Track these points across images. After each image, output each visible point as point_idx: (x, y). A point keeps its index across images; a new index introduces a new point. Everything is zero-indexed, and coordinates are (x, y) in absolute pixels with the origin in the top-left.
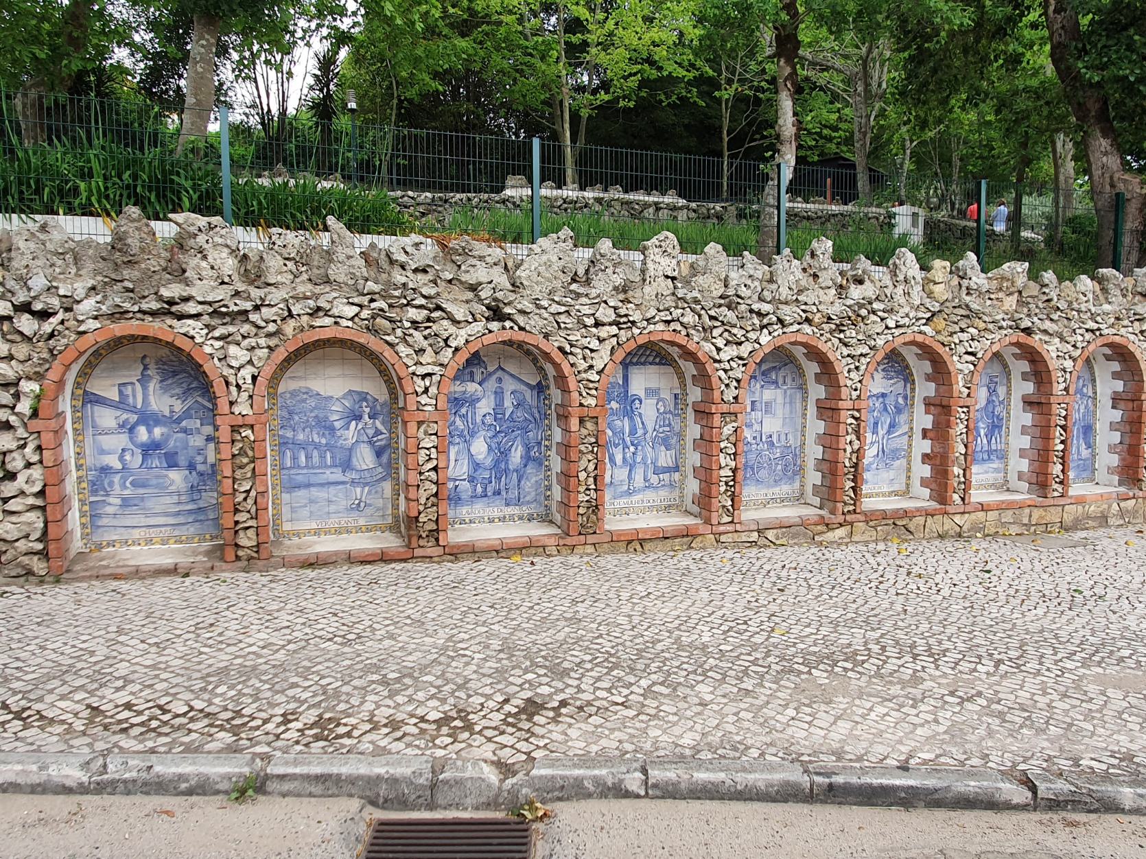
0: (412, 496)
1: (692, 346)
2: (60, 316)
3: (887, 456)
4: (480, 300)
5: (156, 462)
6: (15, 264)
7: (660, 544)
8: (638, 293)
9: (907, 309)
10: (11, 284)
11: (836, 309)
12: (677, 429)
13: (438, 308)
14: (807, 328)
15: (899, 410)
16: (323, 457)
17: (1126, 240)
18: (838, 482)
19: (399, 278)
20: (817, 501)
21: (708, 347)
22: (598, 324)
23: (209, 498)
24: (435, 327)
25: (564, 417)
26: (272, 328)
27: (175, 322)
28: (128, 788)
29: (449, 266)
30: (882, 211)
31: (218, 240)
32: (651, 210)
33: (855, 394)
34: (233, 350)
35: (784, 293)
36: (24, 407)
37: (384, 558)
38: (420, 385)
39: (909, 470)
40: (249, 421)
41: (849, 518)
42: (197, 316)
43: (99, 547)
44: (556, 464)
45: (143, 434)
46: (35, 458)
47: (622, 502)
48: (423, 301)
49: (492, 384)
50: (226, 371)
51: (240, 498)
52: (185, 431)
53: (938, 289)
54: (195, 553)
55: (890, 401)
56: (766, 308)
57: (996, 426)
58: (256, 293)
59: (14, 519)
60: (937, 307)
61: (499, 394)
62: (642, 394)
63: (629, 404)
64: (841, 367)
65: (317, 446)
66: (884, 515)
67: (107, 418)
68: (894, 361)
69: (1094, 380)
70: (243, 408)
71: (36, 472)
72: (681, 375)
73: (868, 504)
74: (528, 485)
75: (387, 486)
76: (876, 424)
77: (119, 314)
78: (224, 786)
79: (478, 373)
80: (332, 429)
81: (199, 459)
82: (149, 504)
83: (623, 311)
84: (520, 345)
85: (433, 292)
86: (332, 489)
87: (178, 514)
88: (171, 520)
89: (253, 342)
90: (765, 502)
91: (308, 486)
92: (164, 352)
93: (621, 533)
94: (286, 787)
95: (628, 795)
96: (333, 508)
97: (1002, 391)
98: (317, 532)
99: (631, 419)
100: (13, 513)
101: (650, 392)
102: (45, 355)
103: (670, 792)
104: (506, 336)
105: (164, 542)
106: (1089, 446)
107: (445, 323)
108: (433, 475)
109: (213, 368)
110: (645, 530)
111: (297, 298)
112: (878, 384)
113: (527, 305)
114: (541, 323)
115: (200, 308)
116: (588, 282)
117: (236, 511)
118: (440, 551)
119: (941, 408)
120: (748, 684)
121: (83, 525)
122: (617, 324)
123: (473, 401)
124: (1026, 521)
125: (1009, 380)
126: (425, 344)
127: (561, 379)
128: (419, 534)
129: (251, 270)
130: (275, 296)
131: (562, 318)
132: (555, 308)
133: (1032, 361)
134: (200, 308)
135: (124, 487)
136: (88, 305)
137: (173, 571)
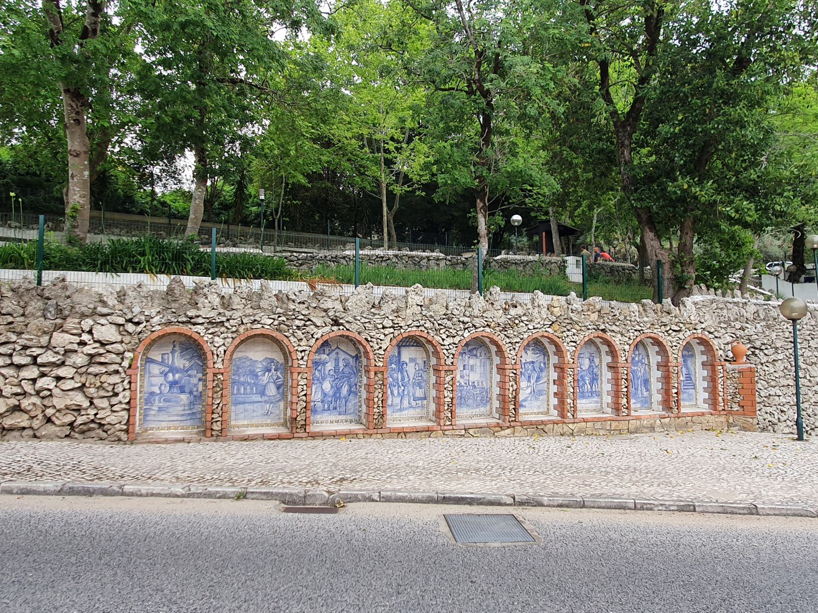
0: (294, 407)
1: (430, 338)
2: (144, 324)
3: (536, 394)
4: (329, 317)
5: (175, 390)
6: (126, 301)
7: (414, 434)
8: (404, 313)
9: (539, 320)
10: (125, 310)
11: (503, 320)
12: (425, 378)
13: (309, 320)
14: (487, 329)
15: (541, 370)
16: (252, 389)
17: (666, 283)
18: (509, 406)
19: (292, 307)
20: (497, 416)
21: (438, 338)
22: (384, 328)
23: (198, 408)
24: (307, 329)
25: (367, 371)
26: (234, 329)
27: (192, 327)
28: (199, 495)
29: (315, 300)
30: (560, 259)
31: (213, 290)
32: (425, 261)
33: (513, 362)
34: (216, 339)
35: (476, 312)
36: (126, 364)
37: (279, 438)
38: (300, 355)
39: (548, 401)
40: (221, 371)
41: (512, 424)
42: (202, 324)
43: (146, 430)
44: (364, 394)
45: (170, 377)
46: (128, 387)
47: (397, 415)
48: (302, 317)
49: (333, 355)
50: (213, 349)
51: (215, 406)
52: (189, 376)
53: (556, 310)
54: (190, 433)
55: (536, 365)
56: (466, 319)
57: (594, 379)
58: (228, 314)
59: (115, 414)
60: (554, 319)
61: (337, 360)
62: (407, 361)
63: (401, 365)
64: (506, 348)
65: (249, 384)
66: (531, 423)
67: (155, 369)
68: (537, 344)
69: (648, 356)
70: (219, 365)
71: (127, 393)
72: (427, 351)
73: (522, 418)
74: (350, 405)
75: (282, 404)
76: (529, 377)
77: (169, 323)
78: (232, 495)
79: (327, 350)
80: (257, 376)
81: (195, 389)
82: (171, 410)
83: (396, 322)
84: (347, 337)
85: (307, 313)
86: (256, 405)
87: (183, 415)
88: (180, 418)
89: (225, 335)
90: (466, 415)
91: (244, 403)
92: (183, 339)
93: (394, 429)
94: (254, 496)
95: (373, 500)
96: (255, 414)
97: (597, 361)
98: (247, 426)
99: (402, 373)
100: (115, 411)
101: (412, 360)
102: (137, 341)
103: (388, 500)
104: (341, 333)
105: (176, 428)
106: (647, 390)
107: (312, 327)
108: (304, 398)
109: (207, 347)
110: (407, 428)
111: (246, 316)
112: (530, 356)
113: (350, 319)
114: (357, 327)
115: (203, 320)
116: (380, 307)
117: (213, 413)
118: (306, 435)
119: (560, 369)
120: (430, 476)
121: (140, 420)
122: (393, 327)
123: (324, 363)
124: (608, 428)
125: (600, 355)
126: (303, 336)
127: (366, 352)
128: (297, 427)
129: (226, 302)
130: (237, 315)
131: (367, 325)
132: (363, 320)
133: (609, 346)
134: (203, 320)
135: (160, 401)
136: (156, 319)
137: (183, 440)
